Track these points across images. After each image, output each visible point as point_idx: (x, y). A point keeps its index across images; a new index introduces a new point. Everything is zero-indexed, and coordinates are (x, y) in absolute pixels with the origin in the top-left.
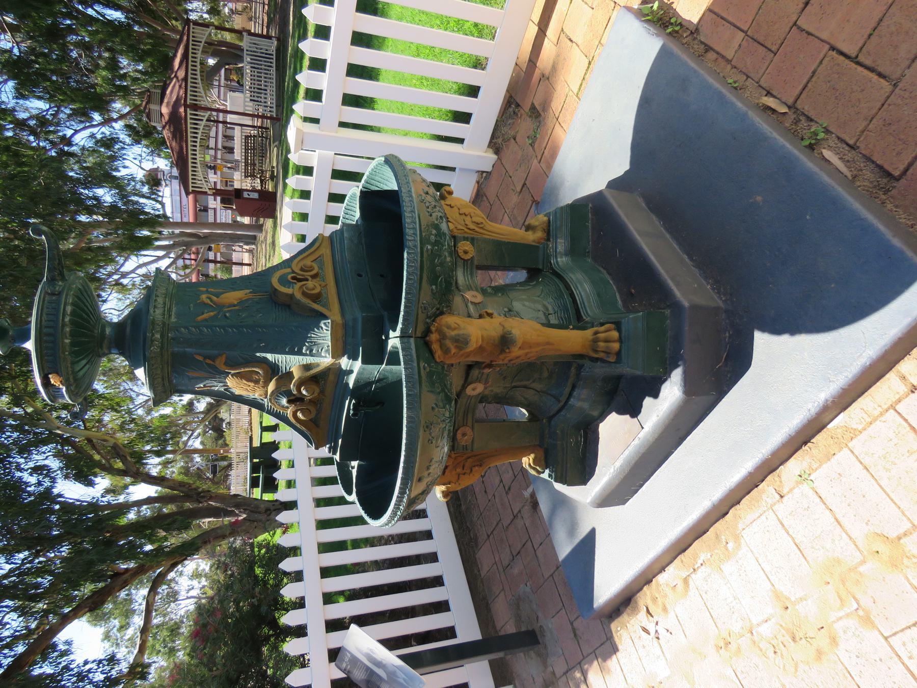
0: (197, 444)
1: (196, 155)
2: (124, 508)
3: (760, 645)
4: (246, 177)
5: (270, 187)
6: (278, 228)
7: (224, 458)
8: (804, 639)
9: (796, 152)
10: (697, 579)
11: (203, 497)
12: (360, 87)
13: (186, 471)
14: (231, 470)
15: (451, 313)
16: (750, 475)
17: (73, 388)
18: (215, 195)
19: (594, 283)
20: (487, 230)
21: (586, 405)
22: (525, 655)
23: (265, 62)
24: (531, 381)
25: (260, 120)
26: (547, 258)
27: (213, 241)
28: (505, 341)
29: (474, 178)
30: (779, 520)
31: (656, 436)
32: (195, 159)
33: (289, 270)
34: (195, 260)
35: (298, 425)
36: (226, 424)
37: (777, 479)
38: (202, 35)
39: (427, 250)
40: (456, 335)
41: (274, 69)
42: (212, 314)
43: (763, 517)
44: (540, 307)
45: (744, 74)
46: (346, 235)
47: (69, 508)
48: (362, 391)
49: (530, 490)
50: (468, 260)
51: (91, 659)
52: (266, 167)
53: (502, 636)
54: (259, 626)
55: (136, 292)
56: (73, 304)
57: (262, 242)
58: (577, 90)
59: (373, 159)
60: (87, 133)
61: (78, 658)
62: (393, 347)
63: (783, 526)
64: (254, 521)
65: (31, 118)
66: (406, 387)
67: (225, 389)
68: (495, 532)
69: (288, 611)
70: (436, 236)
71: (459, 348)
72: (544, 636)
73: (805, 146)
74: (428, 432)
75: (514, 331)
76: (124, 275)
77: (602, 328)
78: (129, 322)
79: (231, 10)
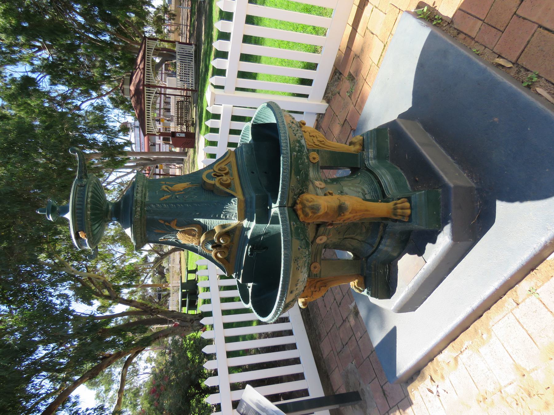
0: (149, 282)
1: (149, 113)
2: (110, 318)
3: (507, 400)
4: (178, 125)
5: (191, 130)
6: (196, 154)
7: (165, 290)
8: (536, 395)
9: (519, 90)
10: (463, 358)
11: (154, 312)
12: (248, 67)
13: (143, 297)
14: (169, 297)
15: (308, 192)
16: (497, 290)
17: (91, 239)
18: (160, 136)
19: (392, 175)
20: (327, 146)
21: (389, 249)
22: (352, 407)
23: (188, 58)
24: (355, 234)
25: (185, 92)
26: (363, 161)
27: (159, 163)
28: (341, 209)
29: (315, 117)
30: (516, 319)
31: (435, 267)
32: (149, 115)
33: (212, 170)
34: (149, 174)
35: (218, 261)
36: (166, 270)
37: (514, 293)
38: (153, 45)
39: (294, 155)
40: (312, 205)
41: (194, 62)
42: (169, 196)
43: (506, 318)
44: (360, 190)
45: (483, 45)
46: (244, 150)
47: (78, 318)
48: (256, 241)
49: (353, 304)
50: (316, 163)
51: (90, 408)
52: (189, 118)
53: (338, 395)
54: (189, 387)
55: (115, 193)
56: (92, 192)
57: (187, 162)
58: (377, 62)
59: (256, 108)
60: (89, 103)
61: (82, 406)
62: (274, 213)
63: (520, 323)
64: (184, 327)
65: (59, 95)
66: (283, 236)
67: (176, 240)
68: (332, 331)
69: (206, 378)
70: (299, 147)
71: (314, 213)
72: (364, 395)
73: (524, 86)
74: (296, 263)
75: (346, 203)
76: (109, 183)
77: (399, 201)
78: (122, 202)
79: (169, 30)
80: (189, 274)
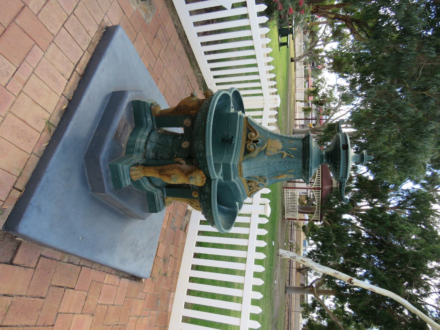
80: (286, 42)
